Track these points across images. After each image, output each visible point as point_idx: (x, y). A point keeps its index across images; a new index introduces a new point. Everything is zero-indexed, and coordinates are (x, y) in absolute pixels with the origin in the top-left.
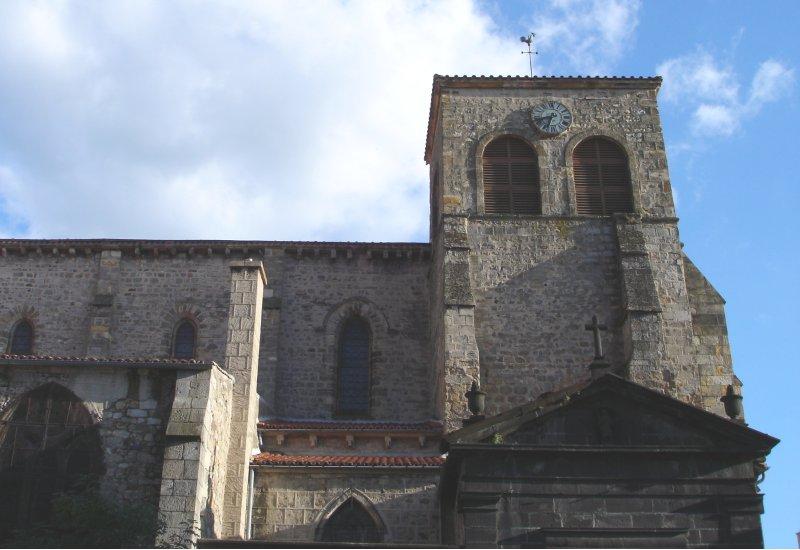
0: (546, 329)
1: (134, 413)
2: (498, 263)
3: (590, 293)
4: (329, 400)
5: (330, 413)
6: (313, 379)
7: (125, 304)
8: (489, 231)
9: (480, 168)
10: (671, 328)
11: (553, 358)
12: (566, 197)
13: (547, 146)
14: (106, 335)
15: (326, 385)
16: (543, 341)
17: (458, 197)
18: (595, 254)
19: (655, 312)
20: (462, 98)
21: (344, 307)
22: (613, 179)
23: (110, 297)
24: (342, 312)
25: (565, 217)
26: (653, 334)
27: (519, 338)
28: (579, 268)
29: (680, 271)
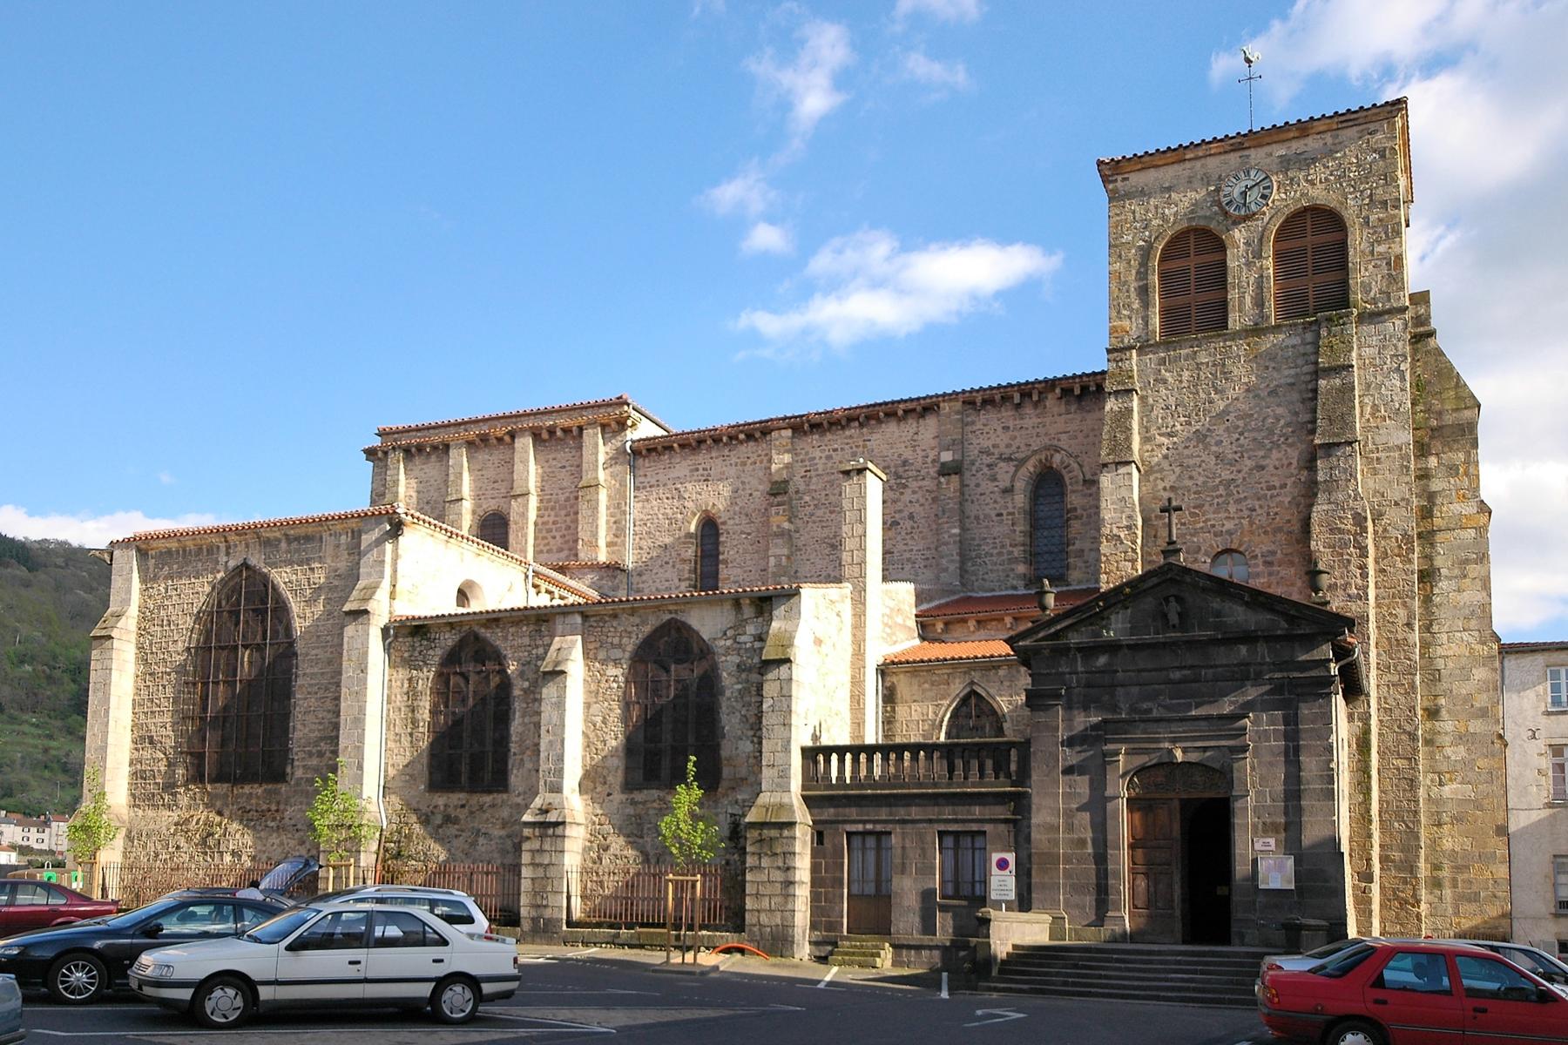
0: (1226, 475)
1: (742, 639)
2: (1172, 401)
3: (1282, 422)
4: (1021, 569)
5: (1071, 560)
6: (1003, 546)
7: (802, 488)
8: (1162, 362)
10: (1382, 455)
11: (1232, 509)
12: (1259, 303)
13: (1239, 235)
14: (786, 525)
15: (1017, 552)
16: (1222, 491)
17: (1126, 323)
18: (1292, 372)
19: (1350, 443)
21: (1032, 461)
22: (1323, 265)
23: (786, 482)
24: (1030, 466)
25: (1256, 331)
26: (1345, 470)
27: (1194, 489)
28: (1270, 394)
29: (1403, 379)
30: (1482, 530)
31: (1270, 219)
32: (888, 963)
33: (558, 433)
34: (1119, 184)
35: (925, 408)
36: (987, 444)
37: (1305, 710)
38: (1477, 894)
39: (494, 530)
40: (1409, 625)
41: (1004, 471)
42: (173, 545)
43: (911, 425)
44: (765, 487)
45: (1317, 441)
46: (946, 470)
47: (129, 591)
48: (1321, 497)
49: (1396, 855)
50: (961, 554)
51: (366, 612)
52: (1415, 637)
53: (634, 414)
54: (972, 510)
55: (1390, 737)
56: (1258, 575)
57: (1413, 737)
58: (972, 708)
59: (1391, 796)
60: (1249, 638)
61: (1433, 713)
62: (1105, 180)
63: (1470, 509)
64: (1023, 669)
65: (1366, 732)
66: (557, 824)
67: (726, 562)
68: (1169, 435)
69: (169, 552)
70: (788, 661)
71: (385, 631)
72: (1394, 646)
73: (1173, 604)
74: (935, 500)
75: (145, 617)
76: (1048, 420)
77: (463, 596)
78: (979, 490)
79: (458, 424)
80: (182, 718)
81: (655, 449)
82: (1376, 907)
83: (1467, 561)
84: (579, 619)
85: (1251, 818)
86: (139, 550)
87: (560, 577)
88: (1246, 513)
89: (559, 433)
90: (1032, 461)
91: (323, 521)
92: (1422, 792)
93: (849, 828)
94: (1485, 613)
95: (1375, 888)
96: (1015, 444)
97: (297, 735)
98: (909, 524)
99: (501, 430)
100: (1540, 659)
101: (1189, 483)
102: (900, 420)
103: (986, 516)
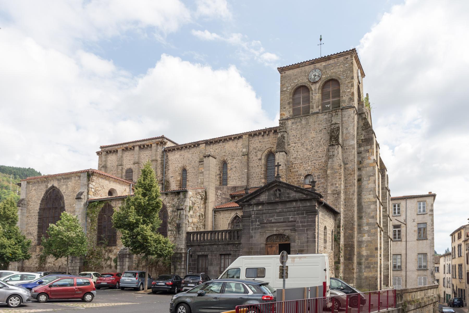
4: (263, 181)
11: (310, 163)
15: (262, 176)
20: (288, 73)
34: (283, 74)
35: (239, 137)
36: (255, 146)
44: (198, 160)
50: (247, 177)
54: (251, 165)
60: (296, 201)
67: (188, 181)
73: (278, 191)
74: (241, 162)
78: (253, 159)
81: (170, 150)
83: (370, 176)
88: (313, 164)
89: (146, 146)
90: (267, 151)
91: (72, 173)
96: (262, 146)
98: (235, 169)
100: (416, 200)
101: (299, 156)
103: (255, 166)
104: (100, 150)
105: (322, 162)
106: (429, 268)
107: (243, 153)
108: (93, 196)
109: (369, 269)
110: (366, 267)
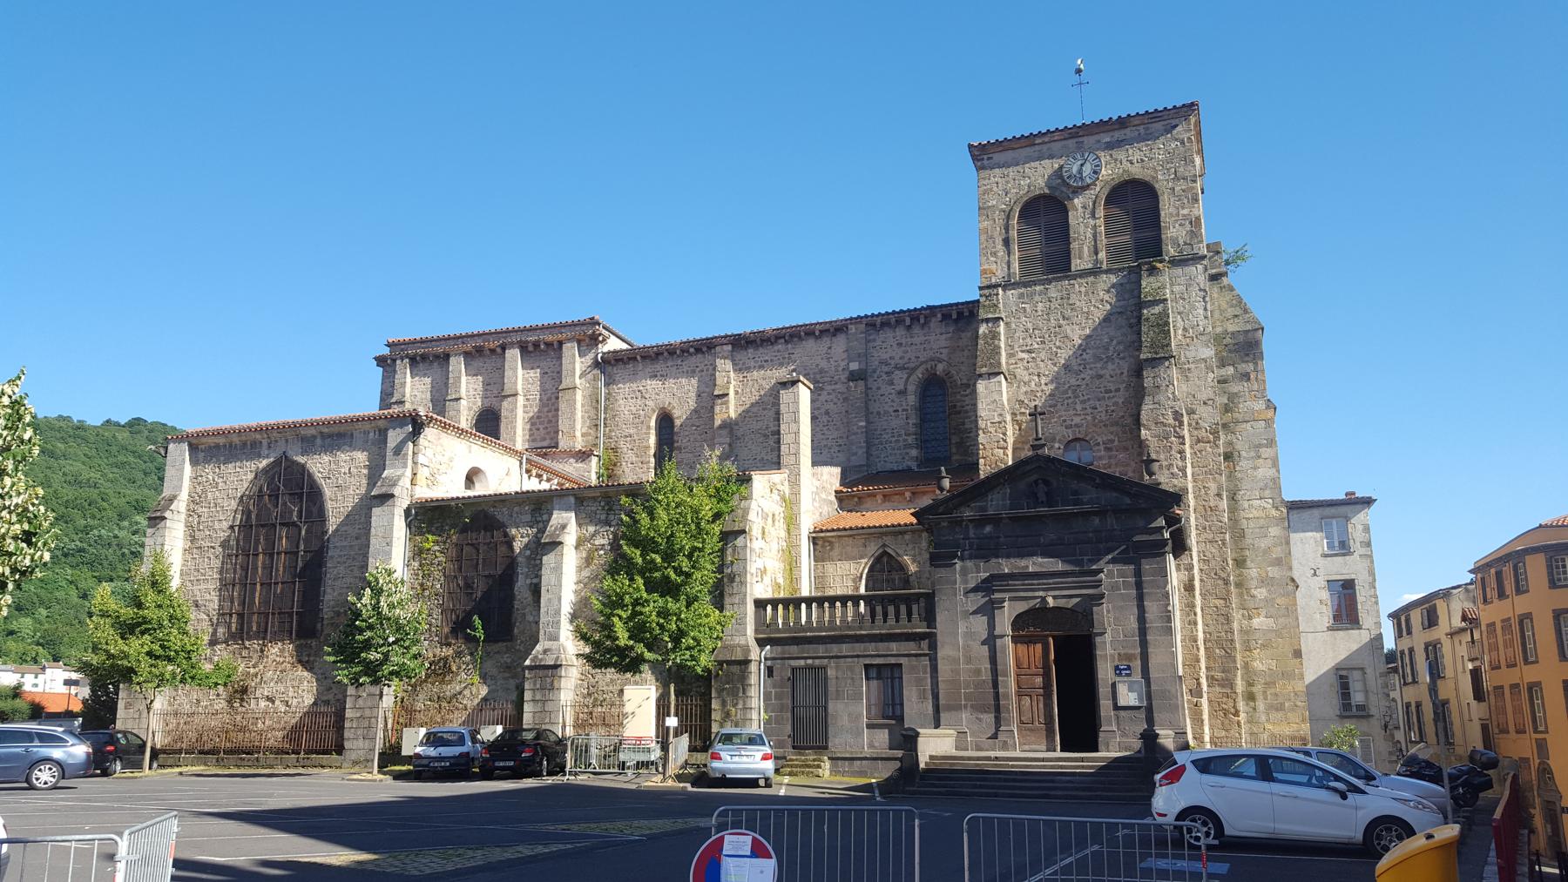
0: (1073, 382)
2: (1030, 325)
4: (914, 452)
9: (1014, 234)
11: (1079, 407)
15: (910, 440)
17: (994, 267)
24: (919, 374)
30: (1269, 422)
31: (1100, 190)
32: (827, 773)
33: (542, 347)
35: (836, 329)
36: (885, 356)
37: (1147, 566)
38: (1282, 704)
39: (489, 424)
40: (1219, 495)
41: (899, 378)
42: (221, 441)
43: (826, 341)
45: (1143, 356)
46: (854, 377)
47: (181, 479)
48: (1148, 399)
49: (1219, 675)
50: (867, 442)
51: (392, 496)
52: (1224, 504)
53: (606, 333)
54: (875, 407)
55: (1209, 582)
56: (1100, 458)
57: (1226, 582)
58: (884, 568)
59: (1212, 629)
61: (1240, 563)
62: (975, 158)
63: (1260, 405)
64: (925, 535)
65: (1192, 580)
66: (556, 667)
67: (679, 449)
68: (1029, 352)
69: (217, 446)
70: (744, 532)
71: (407, 512)
72: (1208, 511)
74: (846, 399)
75: (194, 501)
76: (932, 338)
77: (471, 477)
79: (456, 338)
80: (224, 585)
82: (1206, 717)
83: (1260, 446)
84: (572, 499)
85: (1109, 651)
86: (190, 445)
87: (542, 461)
92: (1236, 626)
93: (795, 663)
94: (1275, 483)
95: (1204, 701)
96: (907, 356)
97: (327, 597)
98: (825, 419)
99: (494, 344)
100: (1316, 512)
102: (817, 338)
103: (886, 412)
104: (386, 351)
105: (1116, 404)
106: (1373, 711)
107: (852, 373)
108: (425, 489)
109: (1280, 714)
110: (1271, 708)
